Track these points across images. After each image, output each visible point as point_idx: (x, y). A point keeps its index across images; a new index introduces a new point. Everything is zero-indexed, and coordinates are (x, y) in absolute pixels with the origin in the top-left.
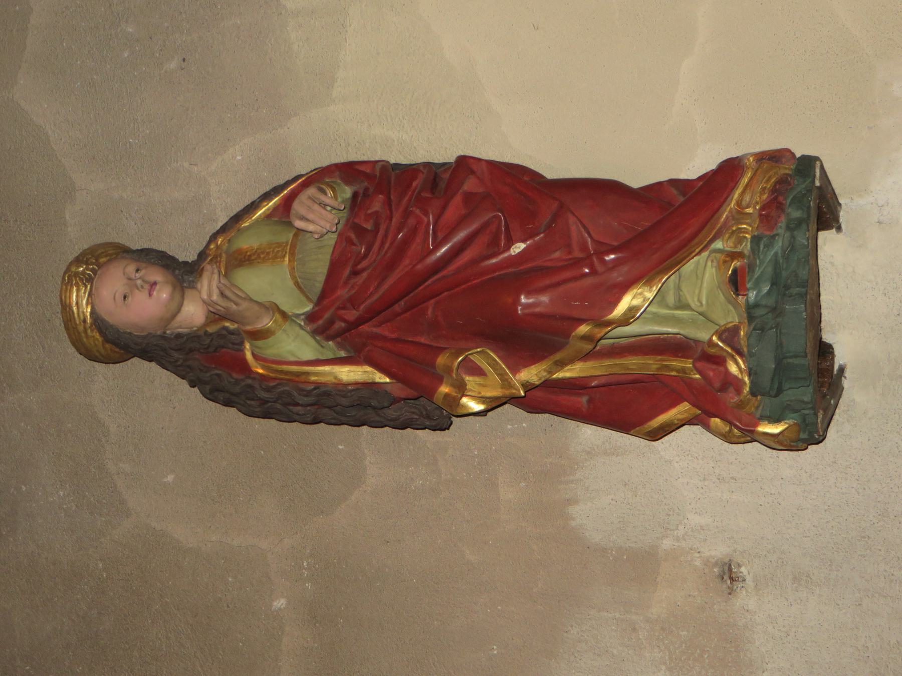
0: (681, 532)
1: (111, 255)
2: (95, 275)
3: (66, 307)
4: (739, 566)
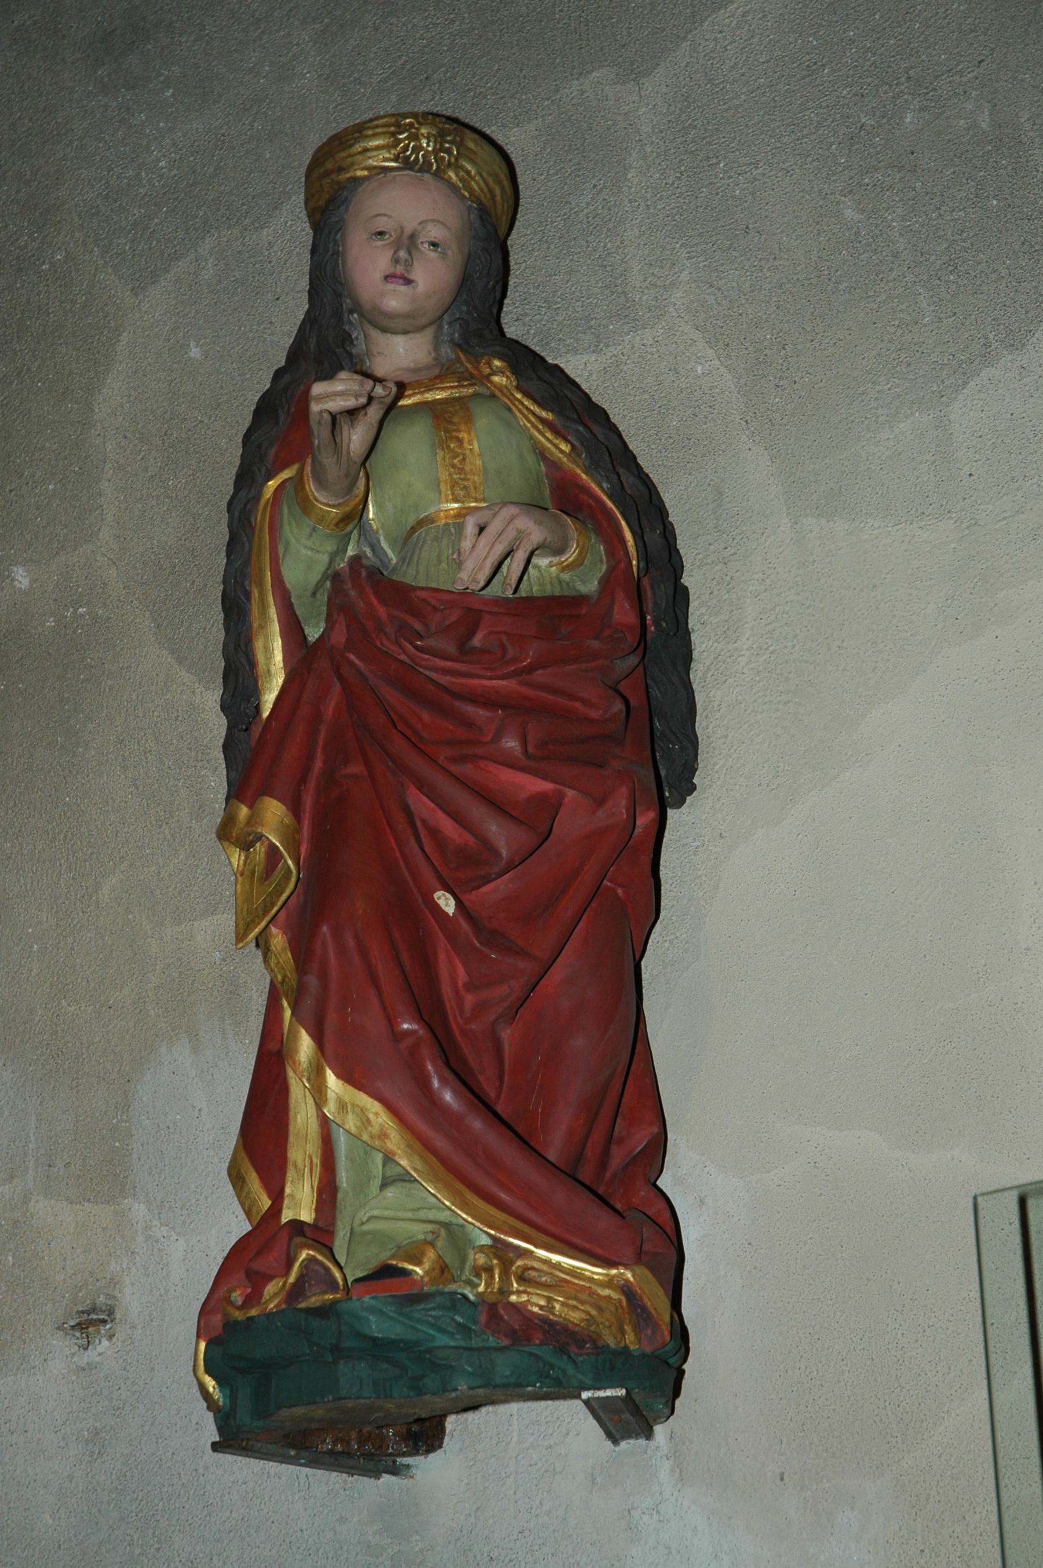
0: (160, 1231)
1: (467, 187)
2: (420, 170)
3: (359, 131)
4: (111, 1337)
